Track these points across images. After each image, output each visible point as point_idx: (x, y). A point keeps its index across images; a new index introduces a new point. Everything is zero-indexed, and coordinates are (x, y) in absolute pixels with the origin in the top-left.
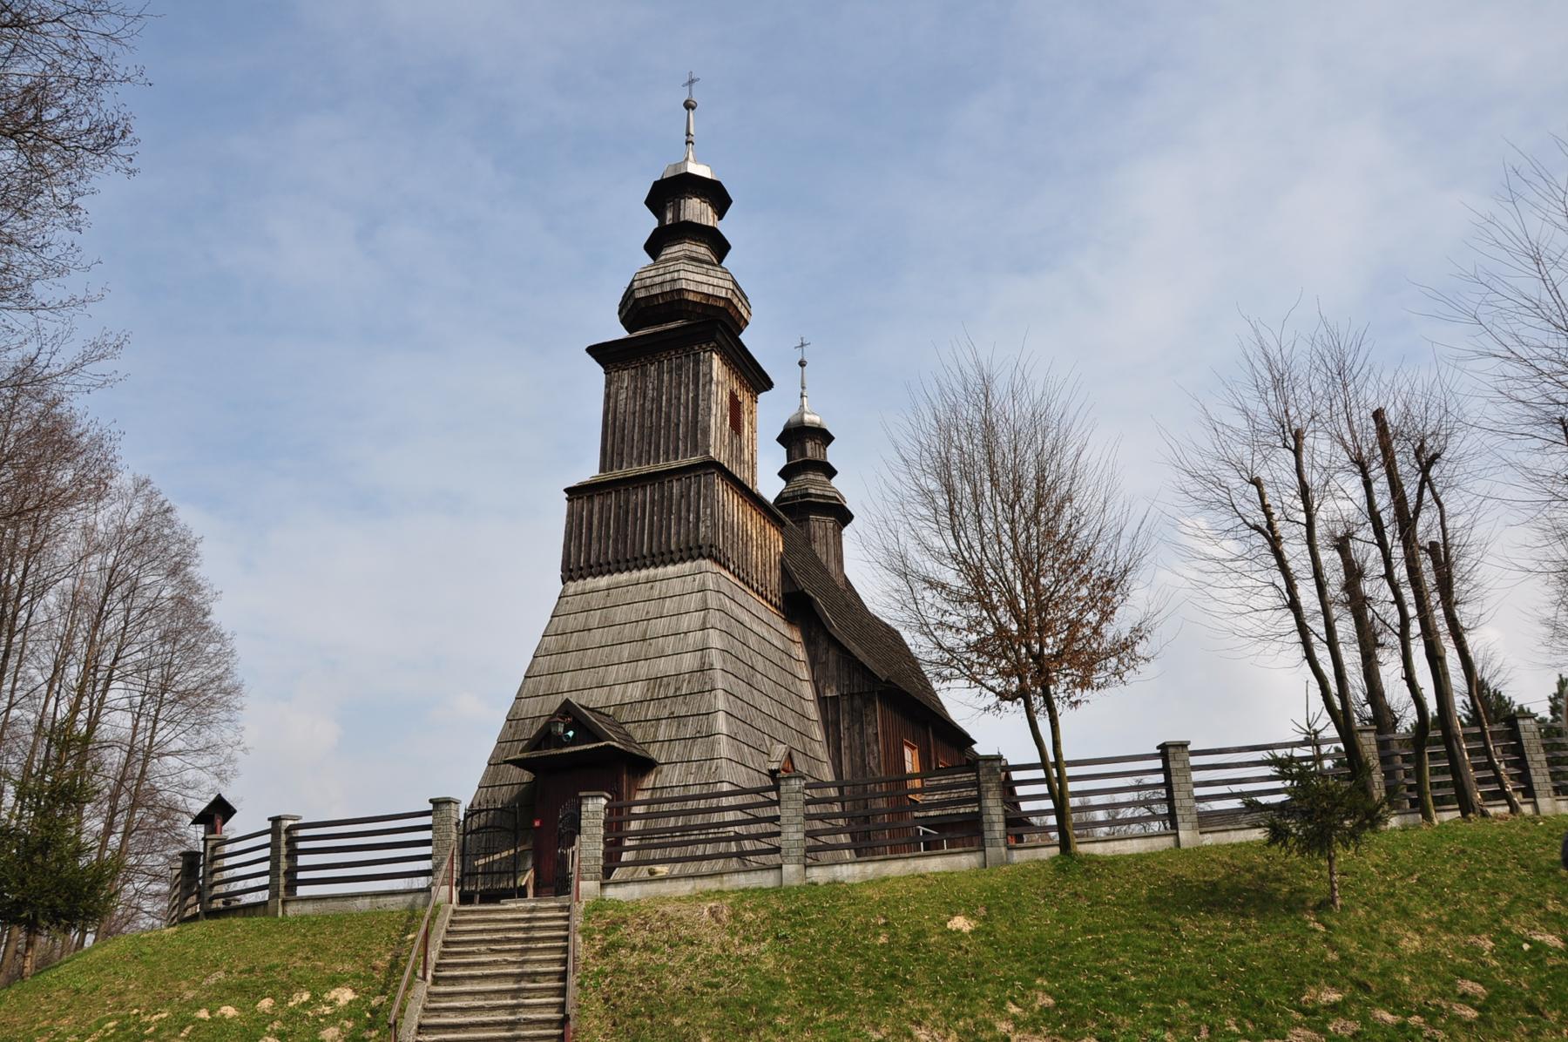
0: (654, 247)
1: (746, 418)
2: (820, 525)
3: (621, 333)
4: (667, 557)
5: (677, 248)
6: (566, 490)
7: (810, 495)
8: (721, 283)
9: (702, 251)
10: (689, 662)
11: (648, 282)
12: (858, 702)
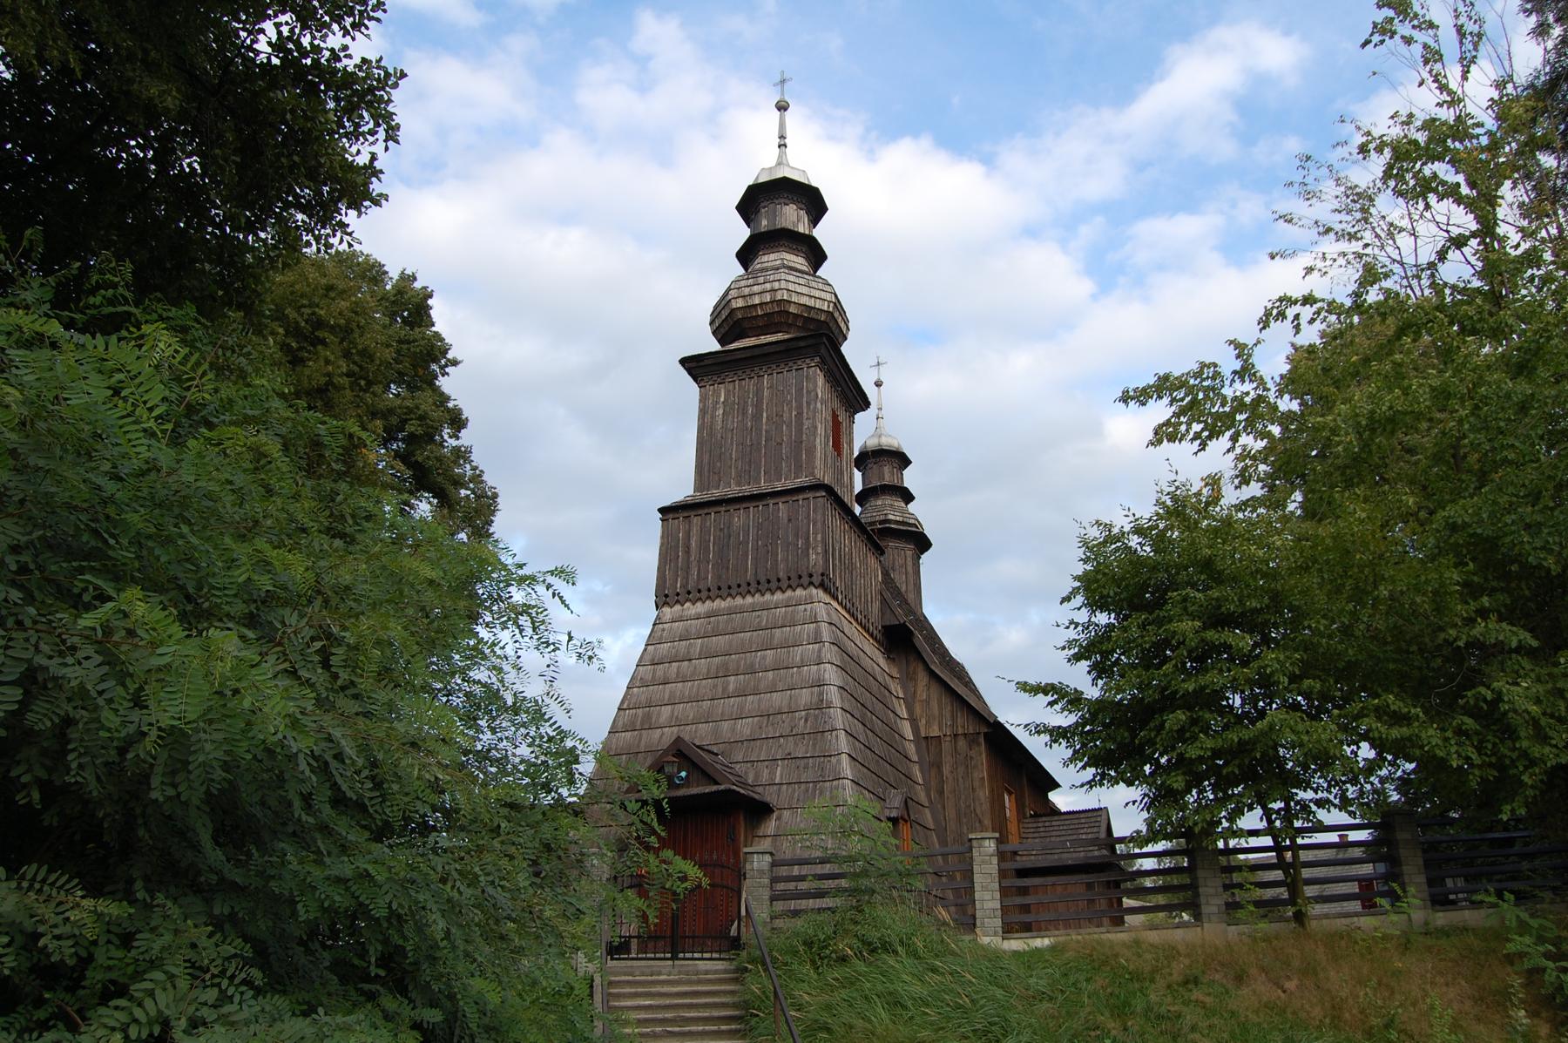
0: (746, 255)
1: (844, 440)
2: (898, 552)
3: (714, 346)
4: (784, 584)
5: (772, 256)
6: (660, 510)
7: (889, 521)
8: (823, 295)
9: (799, 262)
10: (805, 696)
11: (746, 291)
12: (962, 743)
